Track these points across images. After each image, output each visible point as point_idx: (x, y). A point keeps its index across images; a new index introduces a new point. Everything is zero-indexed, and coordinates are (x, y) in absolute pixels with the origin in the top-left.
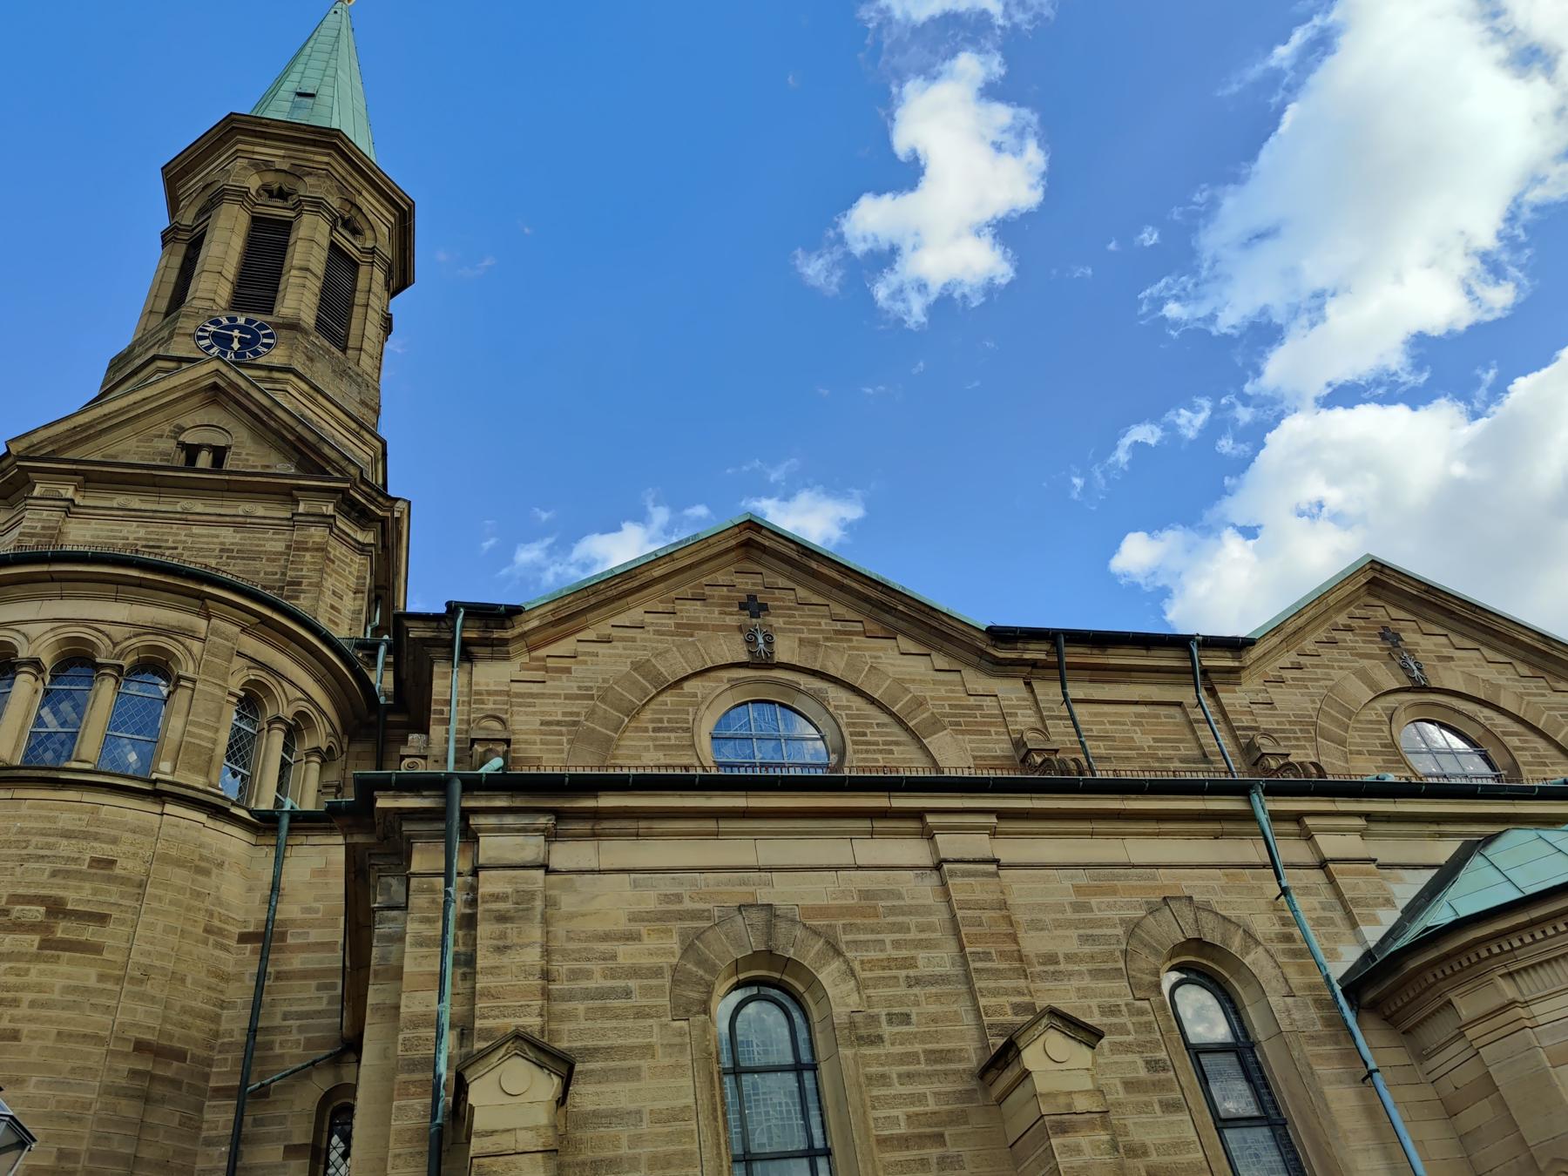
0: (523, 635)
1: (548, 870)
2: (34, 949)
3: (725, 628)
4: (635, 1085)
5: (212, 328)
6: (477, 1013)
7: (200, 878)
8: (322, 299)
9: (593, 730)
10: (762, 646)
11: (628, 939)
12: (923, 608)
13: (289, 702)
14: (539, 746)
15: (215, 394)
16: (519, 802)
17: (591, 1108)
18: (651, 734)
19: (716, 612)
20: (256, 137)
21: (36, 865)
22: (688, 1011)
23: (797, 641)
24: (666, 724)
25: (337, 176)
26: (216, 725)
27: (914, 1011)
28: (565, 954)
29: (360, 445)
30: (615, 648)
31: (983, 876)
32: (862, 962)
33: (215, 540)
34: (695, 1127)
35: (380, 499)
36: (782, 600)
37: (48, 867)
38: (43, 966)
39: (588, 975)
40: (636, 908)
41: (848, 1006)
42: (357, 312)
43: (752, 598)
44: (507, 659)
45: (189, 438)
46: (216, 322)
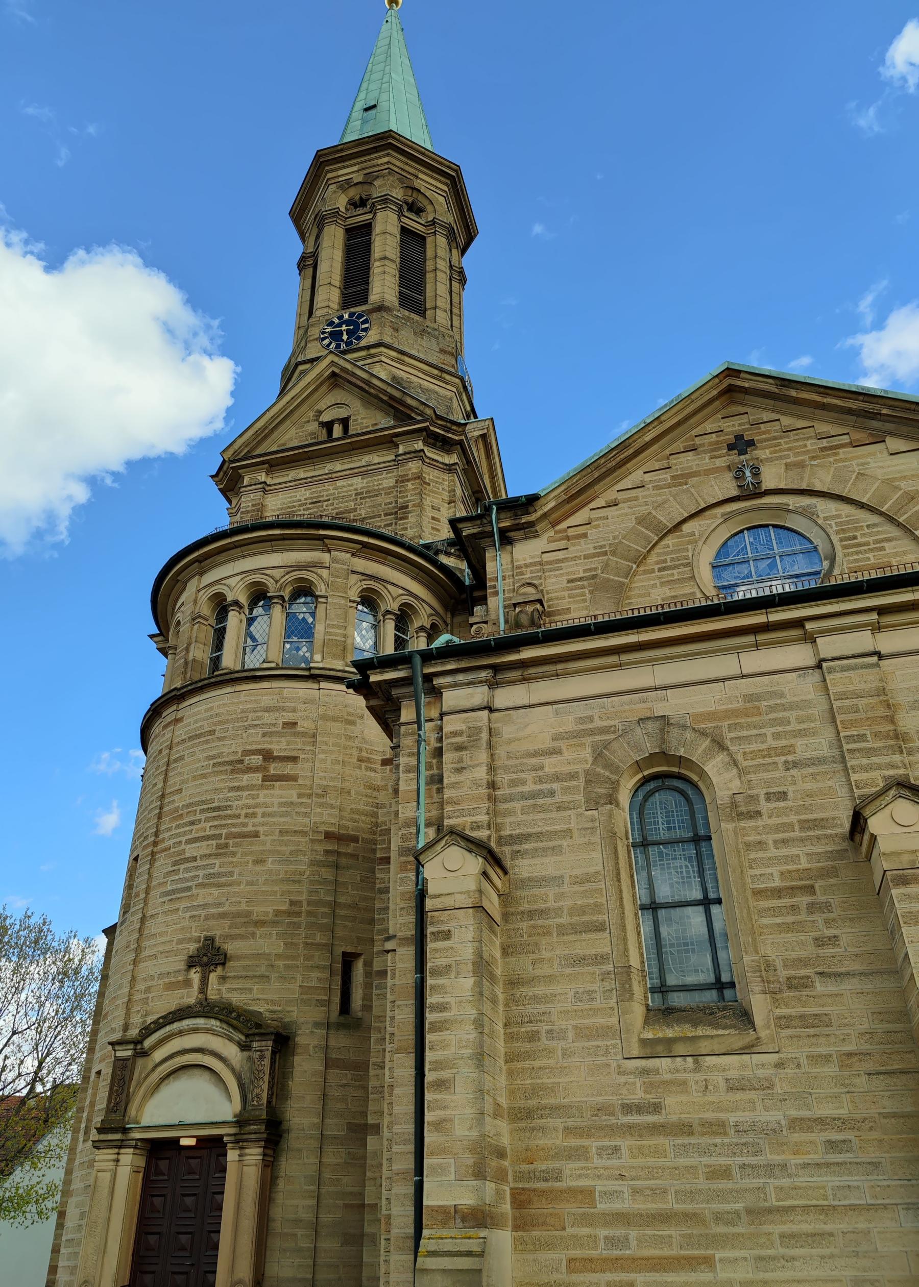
0: (545, 516)
1: (491, 710)
2: (260, 782)
3: (717, 470)
4: (559, 858)
5: (329, 329)
6: (445, 815)
7: (349, 727)
8: (401, 276)
9: (608, 579)
10: (749, 479)
11: (552, 754)
12: (908, 406)
13: (394, 599)
14: (568, 600)
15: (335, 379)
16: (464, 664)
17: (527, 875)
18: (657, 574)
19: (707, 458)
20: (338, 163)
21: (253, 731)
22: (597, 803)
23: (783, 466)
24: (669, 564)
25: (397, 170)
26: (344, 624)
27: (790, 790)
28: (507, 769)
29: (444, 385)
30: (621, 509)
31: (862, 668)
32: (745, 754)
33: (352, 488)
34: (603, 886)
35: (454, 427)
36: (768, 432)
37: (260, 731)
38: (266, 792)
39: (523, 782)
40: (557, 730)
41: (729, 789)
42: (430, 276)
43: (739, 437)
44: (537, 536)
45: (325, 418)
46: (331, 324)
